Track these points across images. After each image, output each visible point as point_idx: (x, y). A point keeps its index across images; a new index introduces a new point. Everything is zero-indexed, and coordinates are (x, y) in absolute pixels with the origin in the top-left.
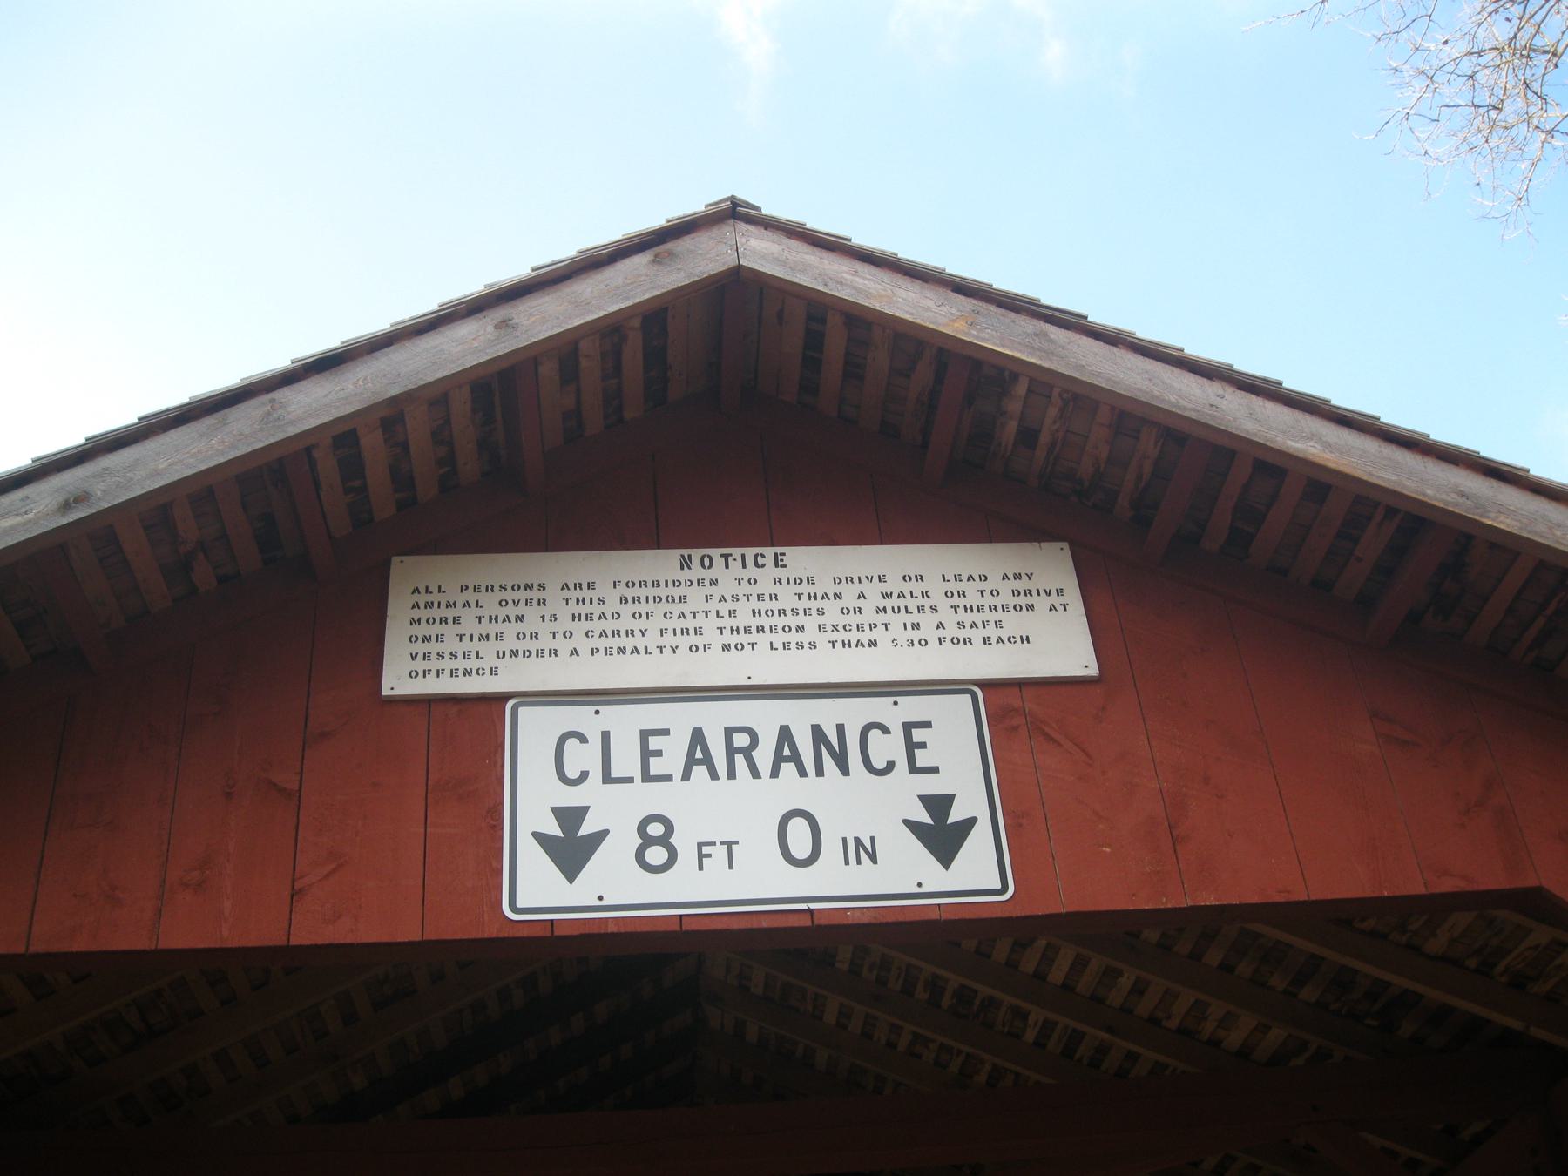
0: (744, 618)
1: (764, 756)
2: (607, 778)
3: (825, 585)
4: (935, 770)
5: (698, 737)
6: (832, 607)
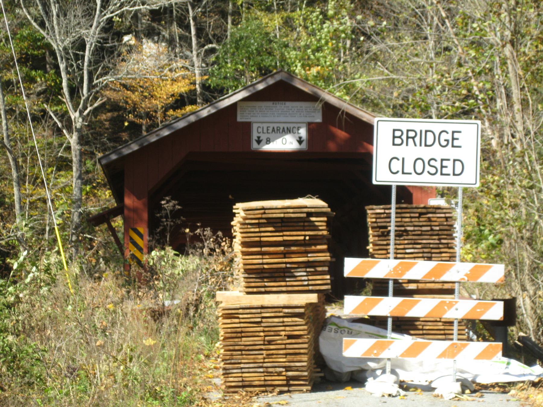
0: (280, 112)
1: (281, 131)
2: (403, 173)
3: (290, 108)
4: (460, 147)
5: (273, 128)
6: (291, 111)
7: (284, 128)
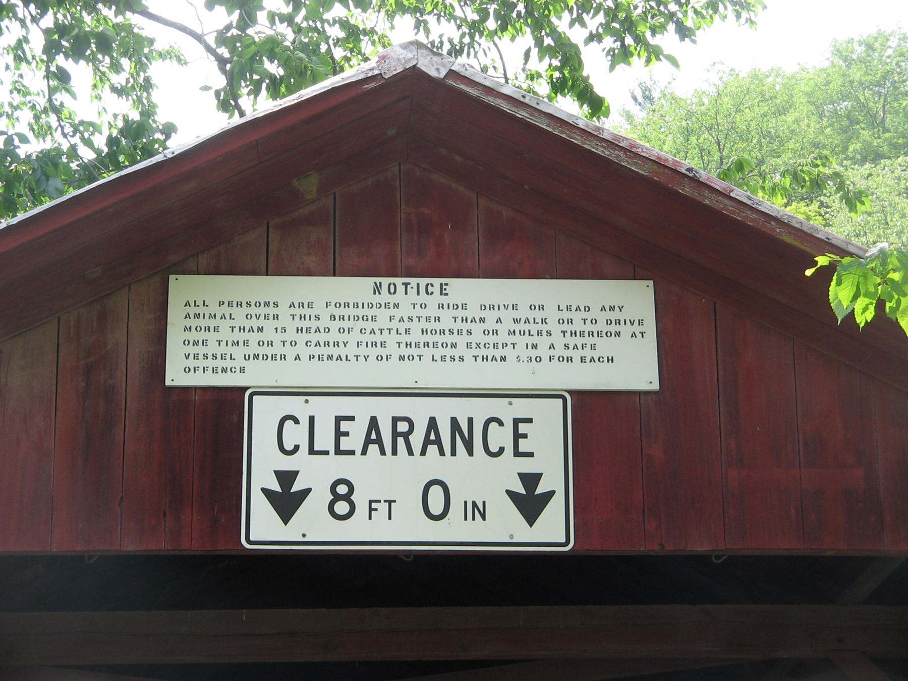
0: (416, 336)
1: (417, 440)
5: (374, 423)
6: (477, 328)
7: (432, 424)
